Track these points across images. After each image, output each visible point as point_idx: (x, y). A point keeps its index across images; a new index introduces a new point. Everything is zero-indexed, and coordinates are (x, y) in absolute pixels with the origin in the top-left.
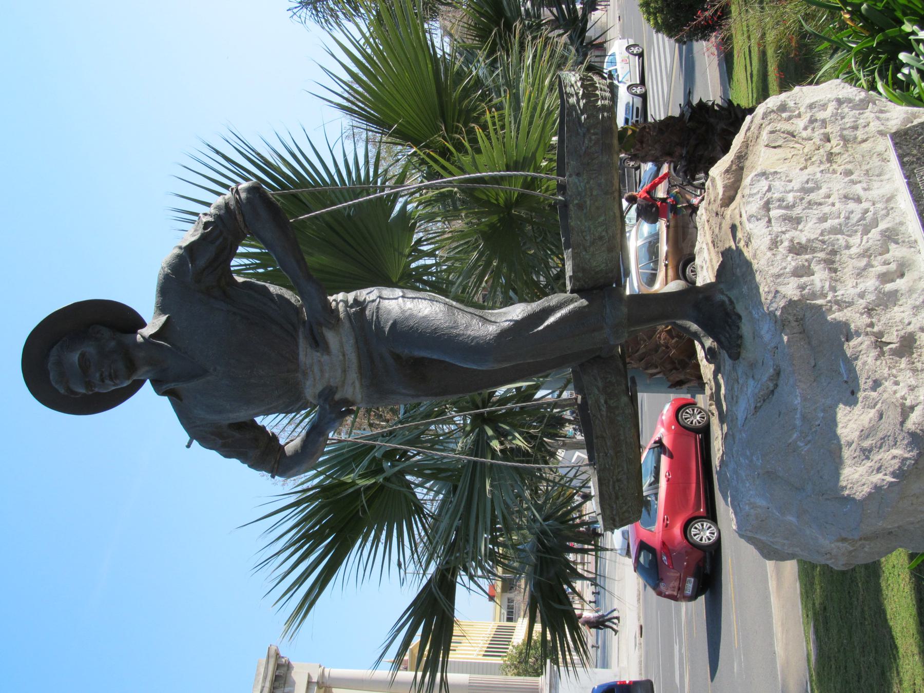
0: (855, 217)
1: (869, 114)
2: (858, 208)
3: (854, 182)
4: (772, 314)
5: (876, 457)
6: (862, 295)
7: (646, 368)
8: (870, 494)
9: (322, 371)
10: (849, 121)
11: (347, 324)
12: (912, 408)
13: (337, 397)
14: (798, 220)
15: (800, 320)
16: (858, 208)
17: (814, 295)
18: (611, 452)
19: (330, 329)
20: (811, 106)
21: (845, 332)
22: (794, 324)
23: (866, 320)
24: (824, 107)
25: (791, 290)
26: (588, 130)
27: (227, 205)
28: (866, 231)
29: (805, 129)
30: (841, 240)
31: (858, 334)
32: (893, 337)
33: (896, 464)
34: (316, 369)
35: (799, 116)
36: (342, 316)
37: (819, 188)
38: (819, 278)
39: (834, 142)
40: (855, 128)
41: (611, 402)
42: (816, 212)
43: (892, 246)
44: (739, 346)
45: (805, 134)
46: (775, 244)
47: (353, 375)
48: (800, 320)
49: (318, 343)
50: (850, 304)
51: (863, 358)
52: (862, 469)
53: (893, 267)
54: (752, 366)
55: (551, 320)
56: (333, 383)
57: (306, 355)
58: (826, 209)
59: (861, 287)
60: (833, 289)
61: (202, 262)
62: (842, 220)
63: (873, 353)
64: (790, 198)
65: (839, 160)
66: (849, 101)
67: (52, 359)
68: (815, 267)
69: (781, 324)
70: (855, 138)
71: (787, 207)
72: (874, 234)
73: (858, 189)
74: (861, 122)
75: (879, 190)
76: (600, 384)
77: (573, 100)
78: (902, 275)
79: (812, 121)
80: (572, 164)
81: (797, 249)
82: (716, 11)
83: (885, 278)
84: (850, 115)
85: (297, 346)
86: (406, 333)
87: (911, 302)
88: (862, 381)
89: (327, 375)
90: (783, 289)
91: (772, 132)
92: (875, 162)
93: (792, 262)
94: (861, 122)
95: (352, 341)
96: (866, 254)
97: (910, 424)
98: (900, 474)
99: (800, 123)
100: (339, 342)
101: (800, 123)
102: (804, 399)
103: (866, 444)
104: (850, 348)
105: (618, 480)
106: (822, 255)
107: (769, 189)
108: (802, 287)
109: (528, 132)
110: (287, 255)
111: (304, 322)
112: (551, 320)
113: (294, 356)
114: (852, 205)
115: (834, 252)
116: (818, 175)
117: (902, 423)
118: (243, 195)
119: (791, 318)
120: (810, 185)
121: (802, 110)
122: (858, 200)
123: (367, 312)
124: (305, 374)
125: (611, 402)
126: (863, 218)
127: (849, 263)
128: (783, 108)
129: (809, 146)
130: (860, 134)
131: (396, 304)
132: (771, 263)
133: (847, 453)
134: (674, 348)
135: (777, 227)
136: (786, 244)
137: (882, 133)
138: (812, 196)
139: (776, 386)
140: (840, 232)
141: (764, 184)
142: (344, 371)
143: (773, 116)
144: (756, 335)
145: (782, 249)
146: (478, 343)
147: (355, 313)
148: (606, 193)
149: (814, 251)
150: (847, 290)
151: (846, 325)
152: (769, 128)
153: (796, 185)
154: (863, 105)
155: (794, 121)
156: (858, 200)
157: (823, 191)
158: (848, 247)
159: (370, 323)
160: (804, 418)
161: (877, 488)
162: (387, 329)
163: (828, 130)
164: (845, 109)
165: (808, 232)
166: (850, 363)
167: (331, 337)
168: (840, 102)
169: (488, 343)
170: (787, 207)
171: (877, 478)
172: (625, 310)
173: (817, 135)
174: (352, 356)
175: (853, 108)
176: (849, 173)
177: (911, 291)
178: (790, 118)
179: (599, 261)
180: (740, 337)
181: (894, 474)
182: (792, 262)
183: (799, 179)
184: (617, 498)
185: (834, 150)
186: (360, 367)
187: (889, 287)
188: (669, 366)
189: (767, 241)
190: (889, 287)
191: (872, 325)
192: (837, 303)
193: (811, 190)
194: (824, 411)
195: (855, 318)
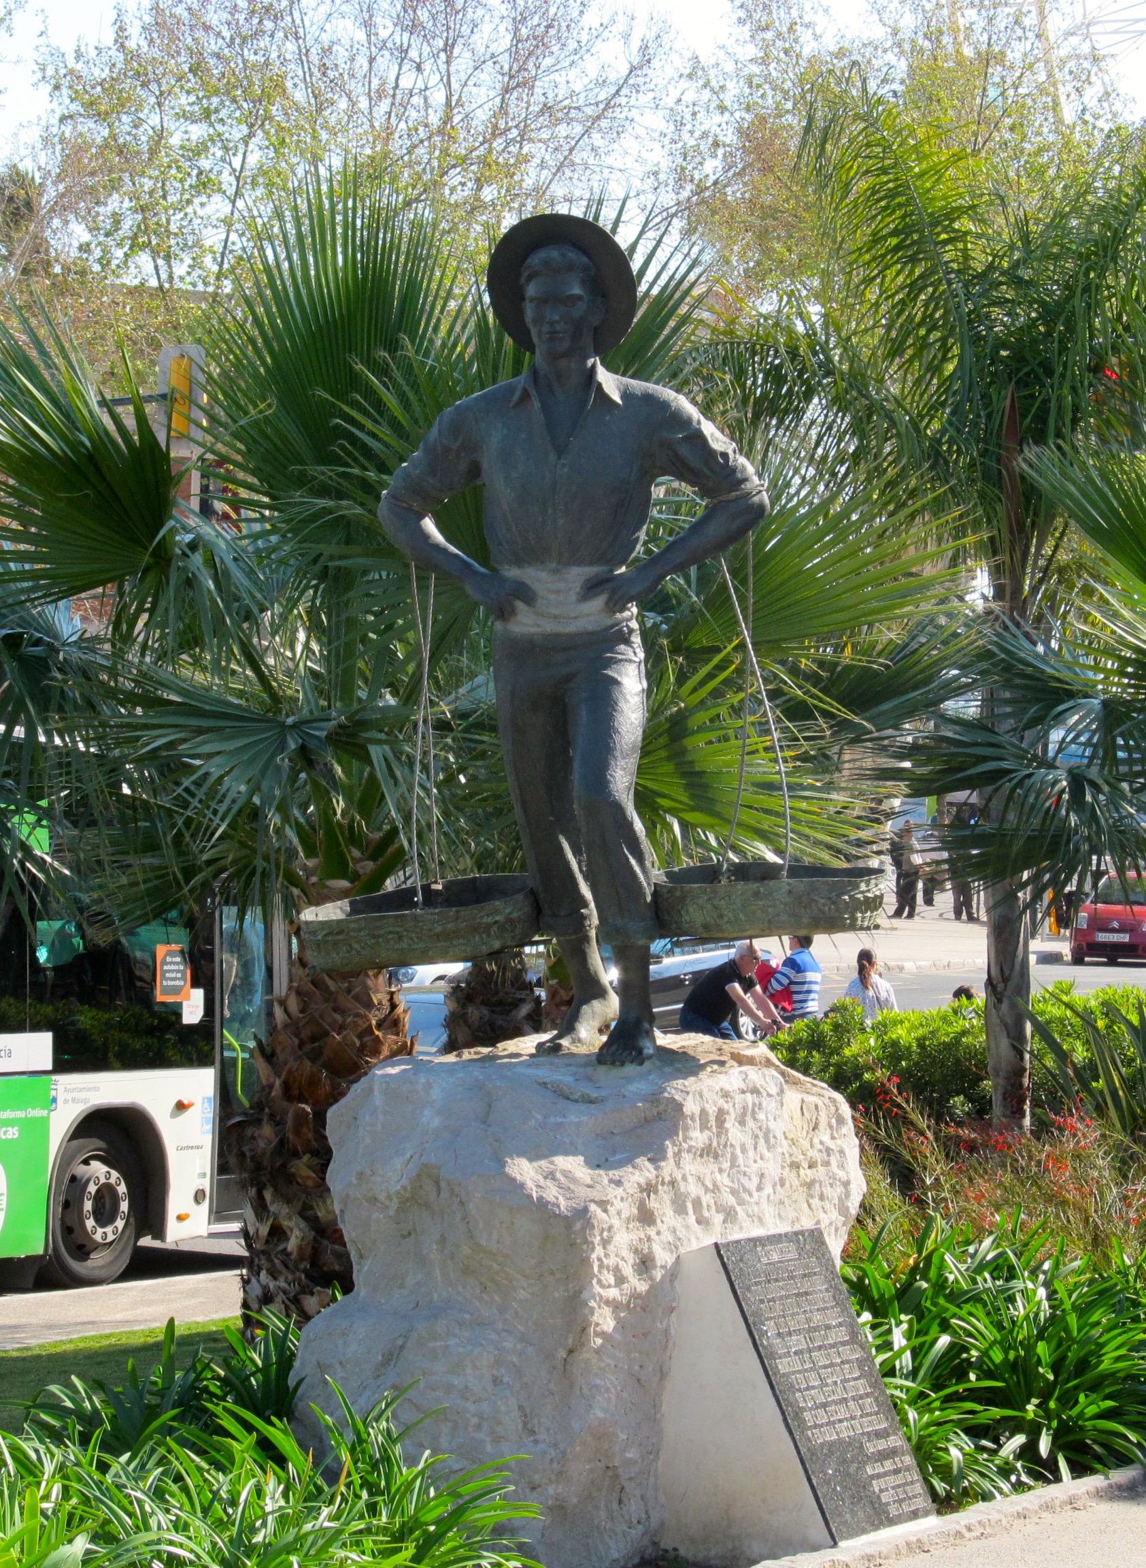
0: (745, 1181)
1: (834, 1215)
2: (752, 1185)
3: (774, 1186)
4: (665, 1090)
5: (549, 1183)
6: (684, 1178)
7: (299, 993)
8: (514, 1180)
9: (558, 592)
10: (828, 1191)
11: (609, 622)
12: (605, 1211)
13: (520, 605)
14: (742, 1123)
15: (659, 1117)
16: (752, 1185)
17: (686, 1129)
18: (439, 929)
19: (607, 603)
20: (841, 1152)
21: (657, 1158)
22: (655, 1112)
23: (667, 1179)
24: (842, 1166)
25: (691, 1107)
26: (834, 903)
27: (746, 480)
28: (734, 1192)
29: (821, 1143)
30: (726, 1165)
31: (657, 1168)
32: (653, 1203)
33: (551, 1199)
34: (561, 586)
35: (833, 1138)
36: (618, 615)
37: (769, 1149)
38: (698, 1138)
39: (809, 1172)
40: (822, 1198)
41: (495, 928)
42: (749, 1143)
43: (721, 1217)
44: (613, 1063)
45: (816, 1141)
46: (726, 1095)
47: (549, 627)
48: (659, 1117)
49: (592, 588)
50: (678, 1165)
51: (637, 1172)
52: (532, 1173)
53: (706, 1214)
54: (589, 1079)
55: (633, 862)
56: (539, 602)
57: (578, 575)
58: (751, 1153)
59: (690, 1179)
60: (689, 1151)
61: (684, 451)
62: (743, 1168)
63: (642, 1181)
64: (761, 1116)
65: (793, 1174)
66: (848, 1195)
67: (573, 255)
68: (707, 1133)
69: (655, 1098)
70: (812, 1196)
71: (753, 1112)
72: (732, 1200)
73: (768, 1190)
74: (827, 1205)
75: (769, 1211)
76: (515, 915)
77: (863, 887)
78: (699, 1222)
79: (828, 1151)
80: (801, 884)
81: (721, 1115)
82: (899, 1106)
83: (697, 1203)
84: (835, 1193)
85: (591, 564)
86: (603, 694)
87: (678, 1226)
88: (616, 1172)
89: (553, 597)
90: (690, 1098)
91: (816, 1107)
92: (792, 1215)
93: (712, 1110)
94: (827, 1205)
95: (590, 628)
96: (716, 1188)
97: (593, 1207)
98: (542, 1204)
99: (826, 1138)
100: (589, 615)
101: (826, 1138)
102: (578, 1125)
103: (558, 1175)
104: (642, 1161)
105: (400, 938)
106: (715, 1144)
107: (769, 1095)
108: (692, 1118)
109: (751, 807)
110: (685, 551)
111: (612, 571)
112: (633, 862)
113: (579, 562)
114: (755, 1180)
115: (716, 1156)
116: (780, 1150)
117: (593, 1201)
118: (756, 499)
119: (661, 1108)
120: (772, 1140)
121: (839, 1142)
122: (759, 1189)
123: (622, 647)
124: (555, 571)
125: (495, 928)
126: (745, 1190)
127: (707, 1169)
128: (841, 1121)
129: (805, 1144)
130: (815, 1202)
131: (631, 682)
132: (710, 1089)
133: (543, 1163)
134: (344, 1038)
135: (739, 1098)
136: (726, 1107)
137: (818, 1222)
138: (762, 1141)
139: (576, 1101)
140: (732, 1167)
141: (773, 1090)
142: (556, 617)
143: (833, 1109)
144: (629, 1079)
145: (721, 1102)
146: (609, 782)
147: (621, 631)
148: (770, 922)
149: (719, 1135)
150: (691, 1165)
151: (664, 1158)
152: (820, 1104)
153: (772, 1125)
154: (843, 1210)
155: (828, 1131)
156: (759, 1189)
157: (765, 1152)
158: (721, 1171)
159: (612, 651)
160: (560, 1125)
161: (522, 1186)
162: (609, 672)
163: (820, 1168)
164: (840, 1190)
165: (735, 1133)
166: (629, 1161)
167: (598, 602)
168: (846, 1184)
169: (610, 794)
170: (753, 1112)
171: (530, 1184)
172: (641, 942)
173: (818, 1157)
174: (571, 628)
175: (840, 1199)
176: (782, 1182)
177: (687, 1227)
178: (831, 1127)
179: (694, 914)
180: (623, 1065)
181: (540, 1198)
182: (712, 1110)
183: (778, 1128)
184: (374, 937)
185: (802, 1172)
186: (557, 635)
187: (690, 1206)
188: (306, 1033)
189: (727, 1087)
190: (690, 1206)
191: (663, 1183)
192: (680, 1151)
193: (767, 1141)
194: (572, 1143)
195: (668, 1167)
